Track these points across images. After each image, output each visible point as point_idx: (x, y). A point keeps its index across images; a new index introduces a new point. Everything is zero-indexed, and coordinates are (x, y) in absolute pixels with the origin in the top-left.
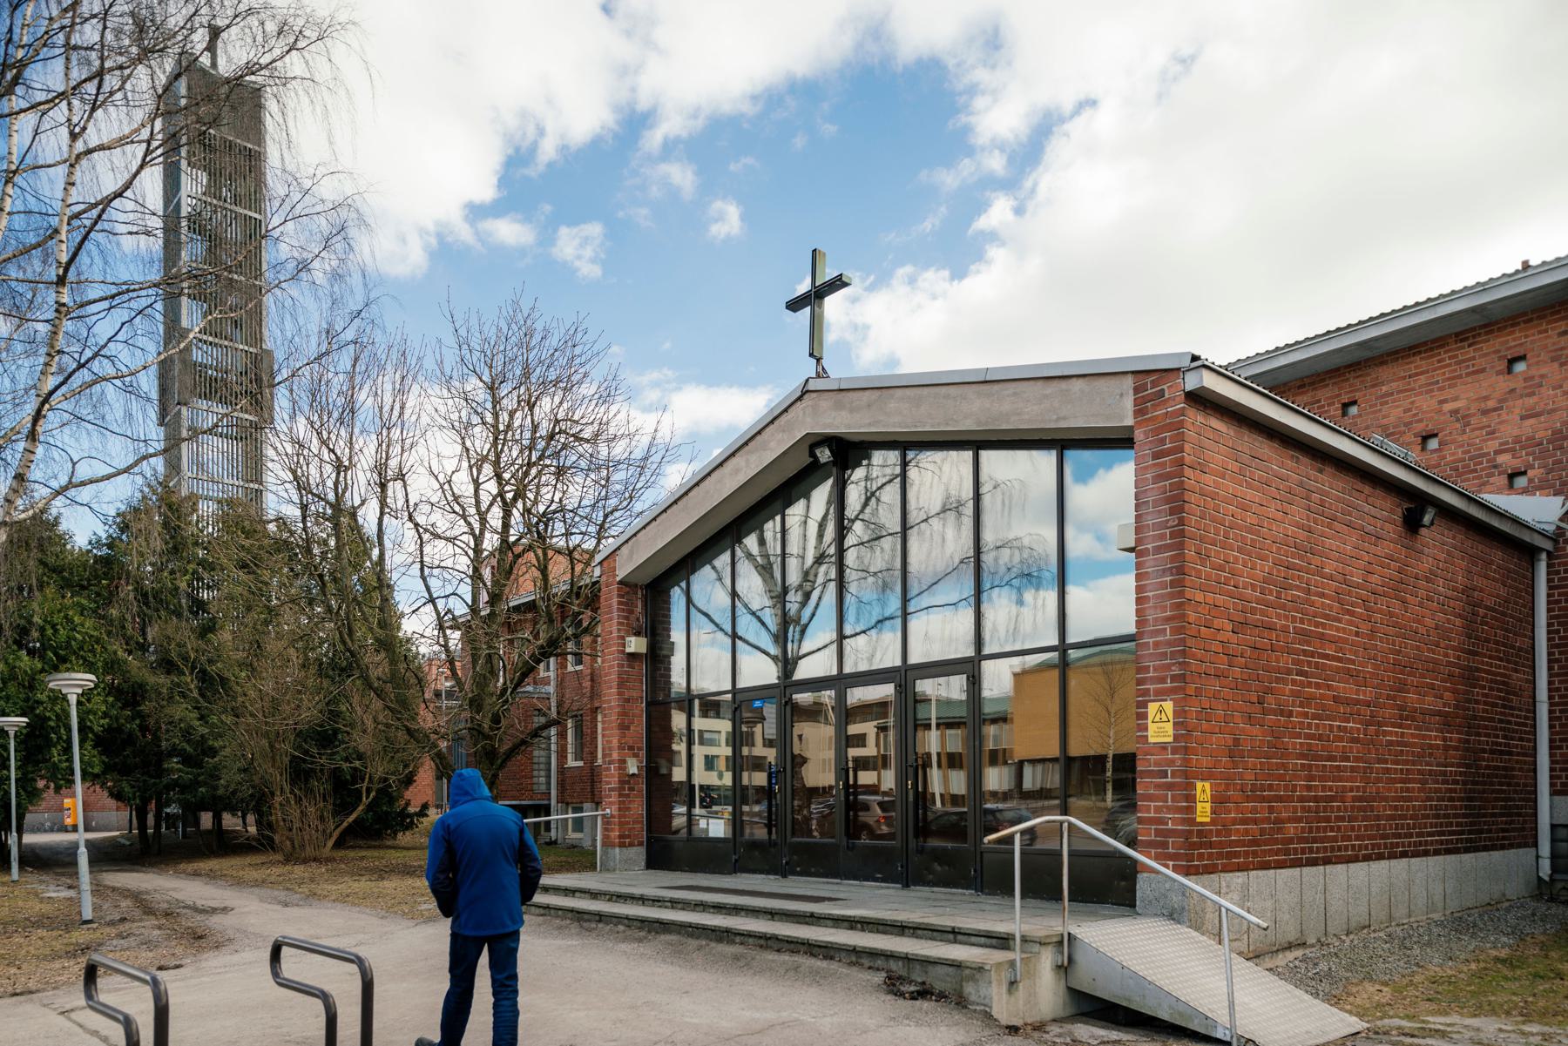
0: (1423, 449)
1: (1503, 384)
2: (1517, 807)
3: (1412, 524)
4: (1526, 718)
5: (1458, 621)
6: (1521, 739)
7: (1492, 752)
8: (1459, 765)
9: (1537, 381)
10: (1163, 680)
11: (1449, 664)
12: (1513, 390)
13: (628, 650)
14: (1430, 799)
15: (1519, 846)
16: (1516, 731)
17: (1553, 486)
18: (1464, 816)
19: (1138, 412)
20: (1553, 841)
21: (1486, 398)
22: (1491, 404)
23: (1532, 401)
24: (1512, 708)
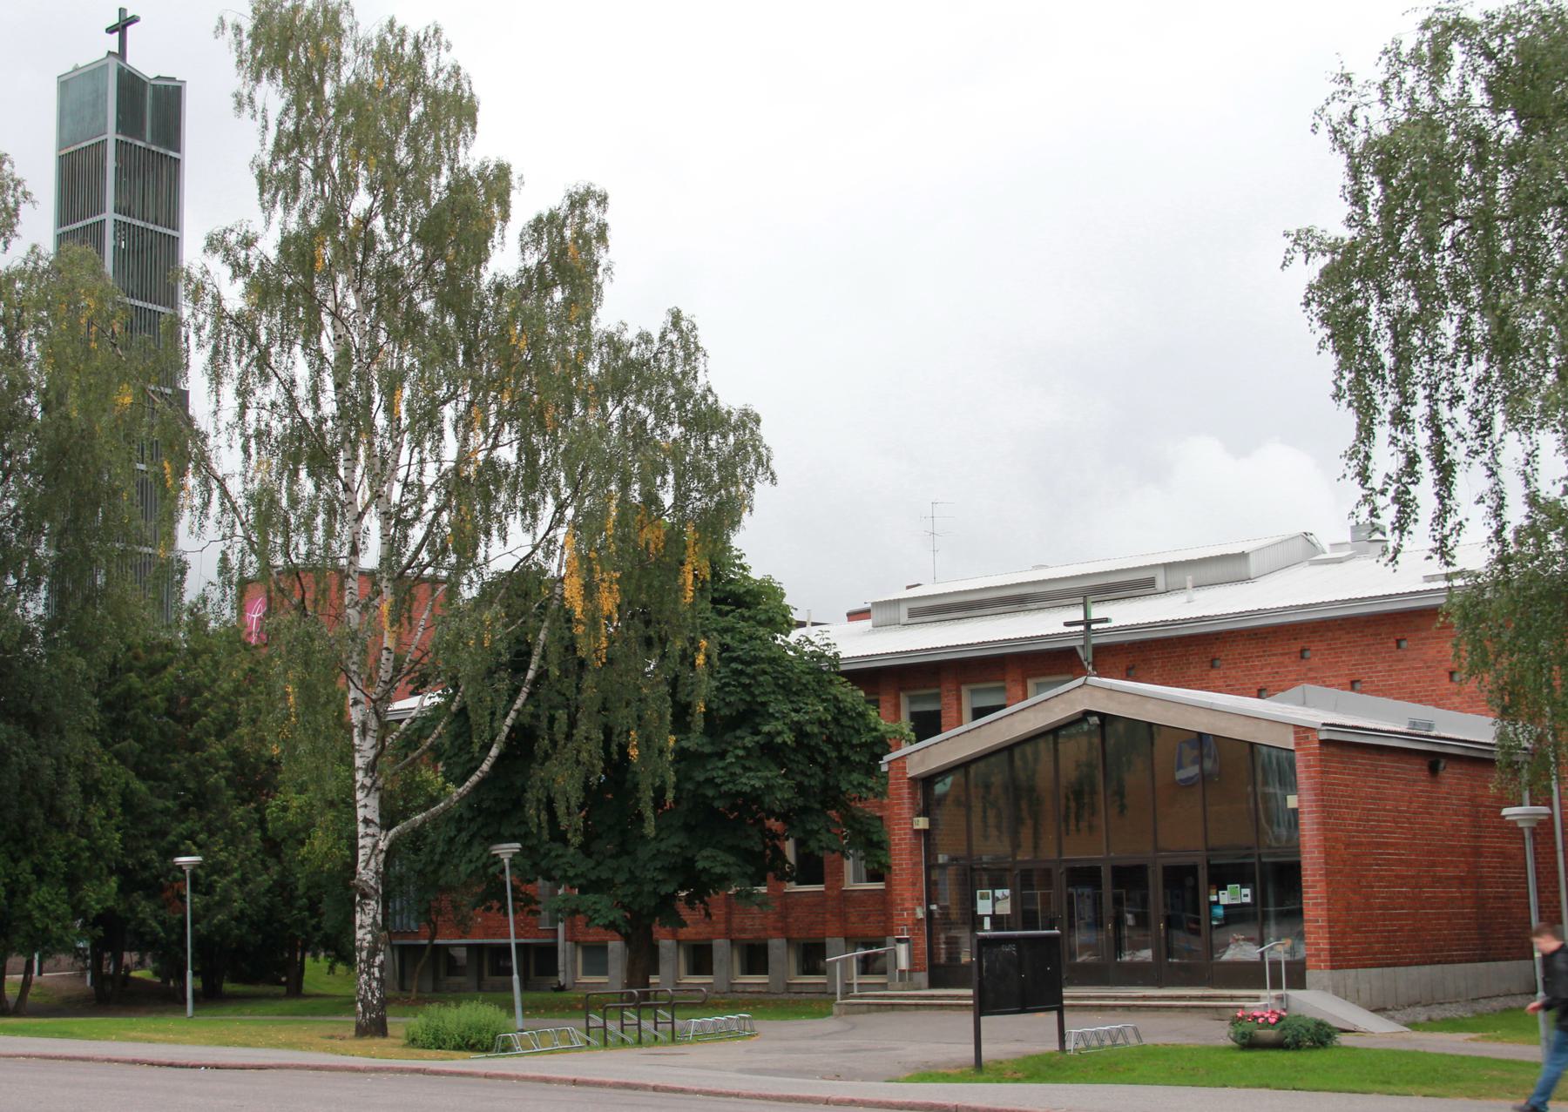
3: (1433, 769)
19: (1297, 744)
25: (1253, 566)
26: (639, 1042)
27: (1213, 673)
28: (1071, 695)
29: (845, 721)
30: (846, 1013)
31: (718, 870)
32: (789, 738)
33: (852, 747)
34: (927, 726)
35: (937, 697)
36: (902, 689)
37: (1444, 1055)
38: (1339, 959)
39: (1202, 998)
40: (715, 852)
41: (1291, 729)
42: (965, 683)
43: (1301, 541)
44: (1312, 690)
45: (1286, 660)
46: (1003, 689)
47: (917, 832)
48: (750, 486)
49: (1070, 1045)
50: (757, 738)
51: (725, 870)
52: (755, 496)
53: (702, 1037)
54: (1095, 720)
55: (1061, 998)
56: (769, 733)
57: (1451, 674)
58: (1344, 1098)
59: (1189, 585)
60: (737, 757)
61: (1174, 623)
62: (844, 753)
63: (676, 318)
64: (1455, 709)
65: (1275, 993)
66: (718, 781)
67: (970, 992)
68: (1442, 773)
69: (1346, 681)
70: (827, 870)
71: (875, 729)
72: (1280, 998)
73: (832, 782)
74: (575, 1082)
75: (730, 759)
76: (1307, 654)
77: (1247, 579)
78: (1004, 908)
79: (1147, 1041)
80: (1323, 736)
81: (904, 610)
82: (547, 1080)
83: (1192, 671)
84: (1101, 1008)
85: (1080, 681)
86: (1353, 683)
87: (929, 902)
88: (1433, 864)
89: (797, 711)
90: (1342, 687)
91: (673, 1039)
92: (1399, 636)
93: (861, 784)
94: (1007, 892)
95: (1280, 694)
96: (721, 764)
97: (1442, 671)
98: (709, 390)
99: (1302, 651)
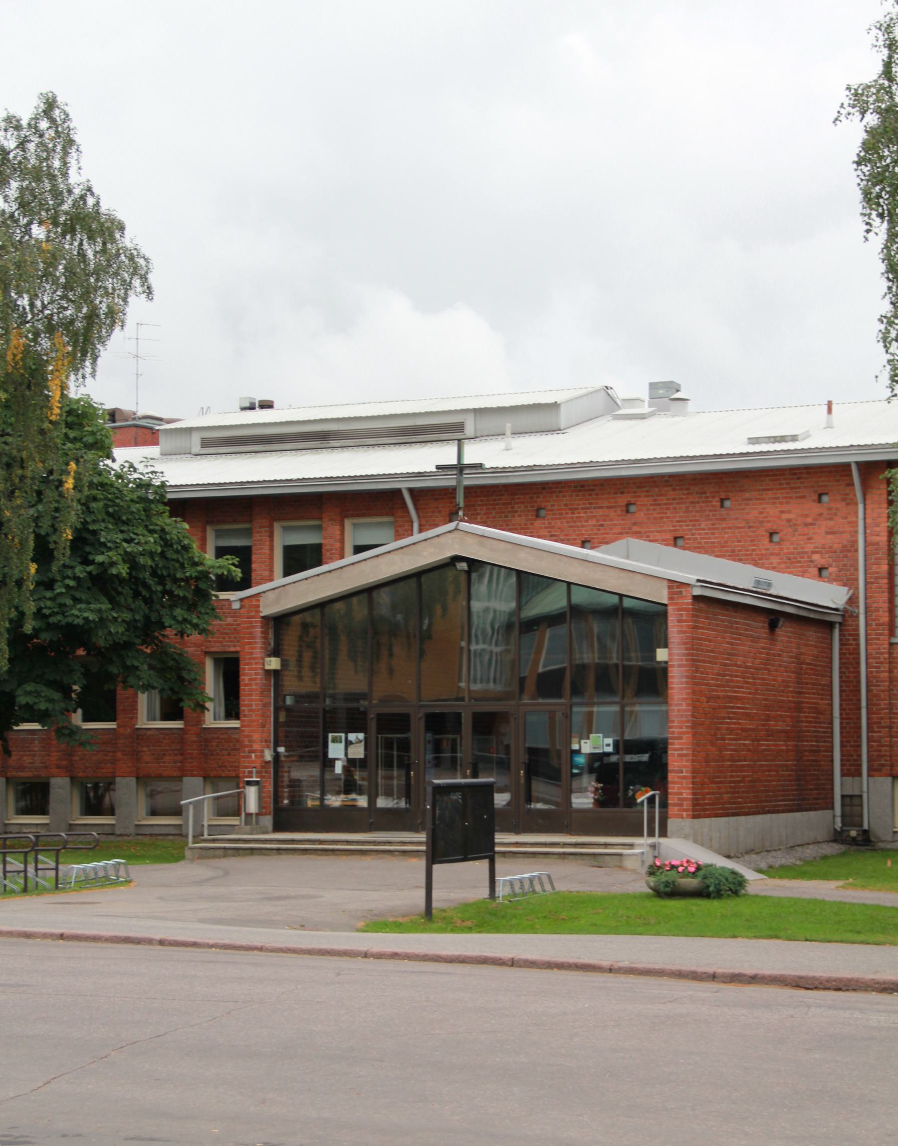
0: (771, 541)
1: (815, 508)
2: (823, 784)
3: (773, 627)
4: (828, 728)
5: (793, 675)
6: (825, 742)
7: (810, 751)
8: (794, 760)
9: (834, 511)
10: (681, 727)
11: (790, 701)
12: (821, 514)
13: (267, 667)
14: (780, 781)
15: (824, 809)
16: (822, 737)
17: (842, 580)
18: (796, 790)
19: (670, 599)
20: (843, 805)
21: (807, 516)
22: (809, 520)
23: (831, 523)
24: (820, 723)
25: (564, 417)
26: (25, 890)
27: (538, 523)
28: (442, 540)
29: (170, 554)
30: (201, 857)
31: (43, 706)
32: (123, 570)
33: (175, 580)
34: (299, 559)
35: (249, 533)
36: (208, 522)
37: (864, 905)
38: (700, 810)
39: (576, 845)
40: (40, 687)
41: (665, 584)
42: (279, 519)
43: (603, 393)
44: (635, 544)
45: (612, 513)
46: (319, 528)
47: (268, 672)
48: (125, 300)
49: (500, 891)
50: (89, 569)
51: (49, 706)
52: (128, 310)
53: (87, 882)
54: (464, 566)
55: (493, 844)
56: (102, 564)
57: (771, 534)
58: (683, 939)
59: (508, 432)
60: (67, 587)
61: (504, 470)
62: (168, 587)
63: (50, 104)
64: (774, 569)
65: (651, 840)
66: (46, 612)
67: (422, 837)
68: (778, 631)
69: (669, 536)
70: (119, 707)
71: (201, 564)
72: (653, 846)
73: (154, 617)
74: (62, 936)
75: (59, 589)
76: (632, 508)
77: (556, 430)
78: (358, 752)
79: (561, 887)
80: (697, 592)
81: (196, 439)
82: (28, 935)
83: (517, 520)
84: (305, 851)
85: (452, 526)
86: (676, 538)
87: (277, 744)
88: (768, 718)
89: (129, 541)
90: (665, 542)
91: (57, 888)
92: (723, 496)
93: (185, 620)
94: (361, 736)
95: (604, 547)
96: (48, 594)
97: (763, 532)
98: (89, 189)
99: (628, 505)
